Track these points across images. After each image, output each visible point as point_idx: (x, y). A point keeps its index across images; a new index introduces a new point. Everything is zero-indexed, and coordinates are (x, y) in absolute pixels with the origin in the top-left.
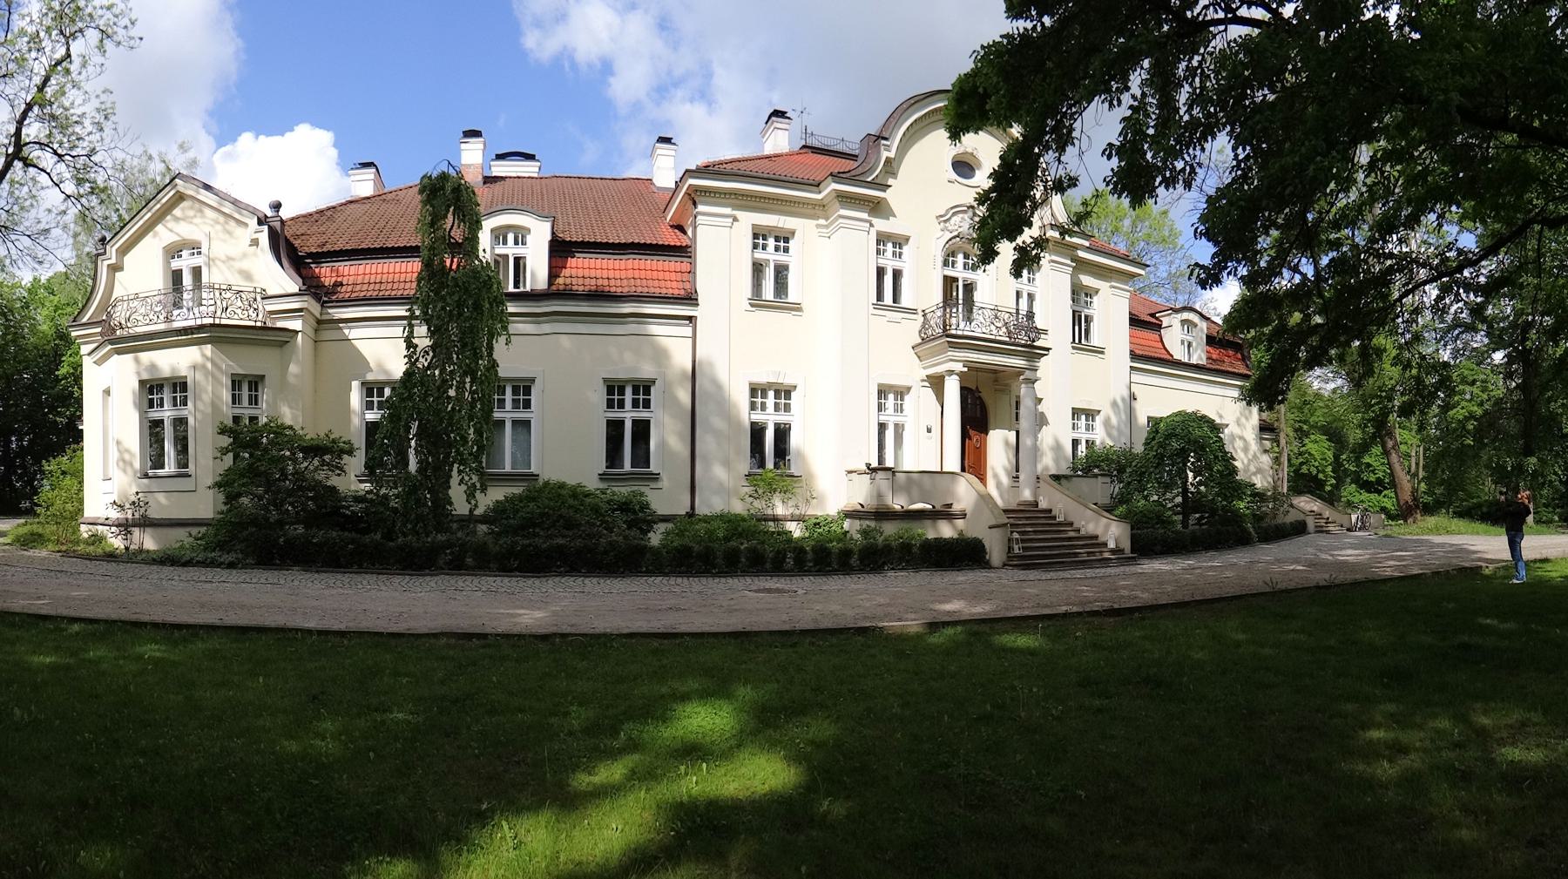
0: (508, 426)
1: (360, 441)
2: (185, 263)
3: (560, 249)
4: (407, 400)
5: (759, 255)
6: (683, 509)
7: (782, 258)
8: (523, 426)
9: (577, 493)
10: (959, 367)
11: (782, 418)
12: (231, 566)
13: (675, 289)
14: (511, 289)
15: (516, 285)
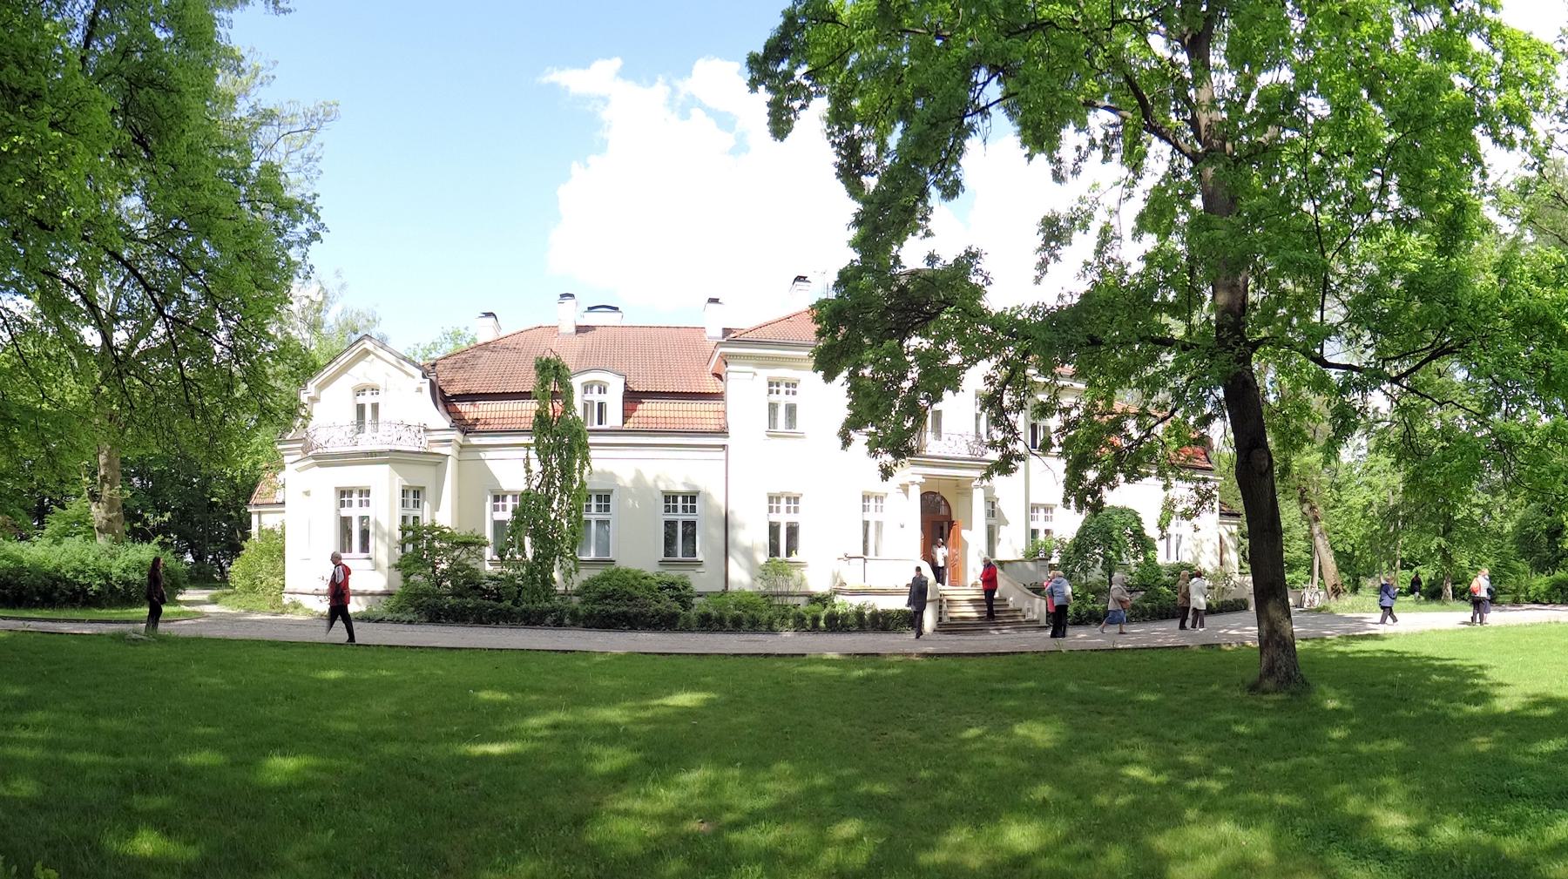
0: (593, 524)
1: (489, 535)
2: (367, 400)
3: (632, 398)
4: (531, 511)
5: (774, 398)
6: (719, 587)
7: (791, 399)
8: (603, 523)
9: (639, 577)
10: (919, 479)
11: (792, 518)
12: (410, 622)
13: (712, 425)
14: (596, 426)
15: (600, 423)
